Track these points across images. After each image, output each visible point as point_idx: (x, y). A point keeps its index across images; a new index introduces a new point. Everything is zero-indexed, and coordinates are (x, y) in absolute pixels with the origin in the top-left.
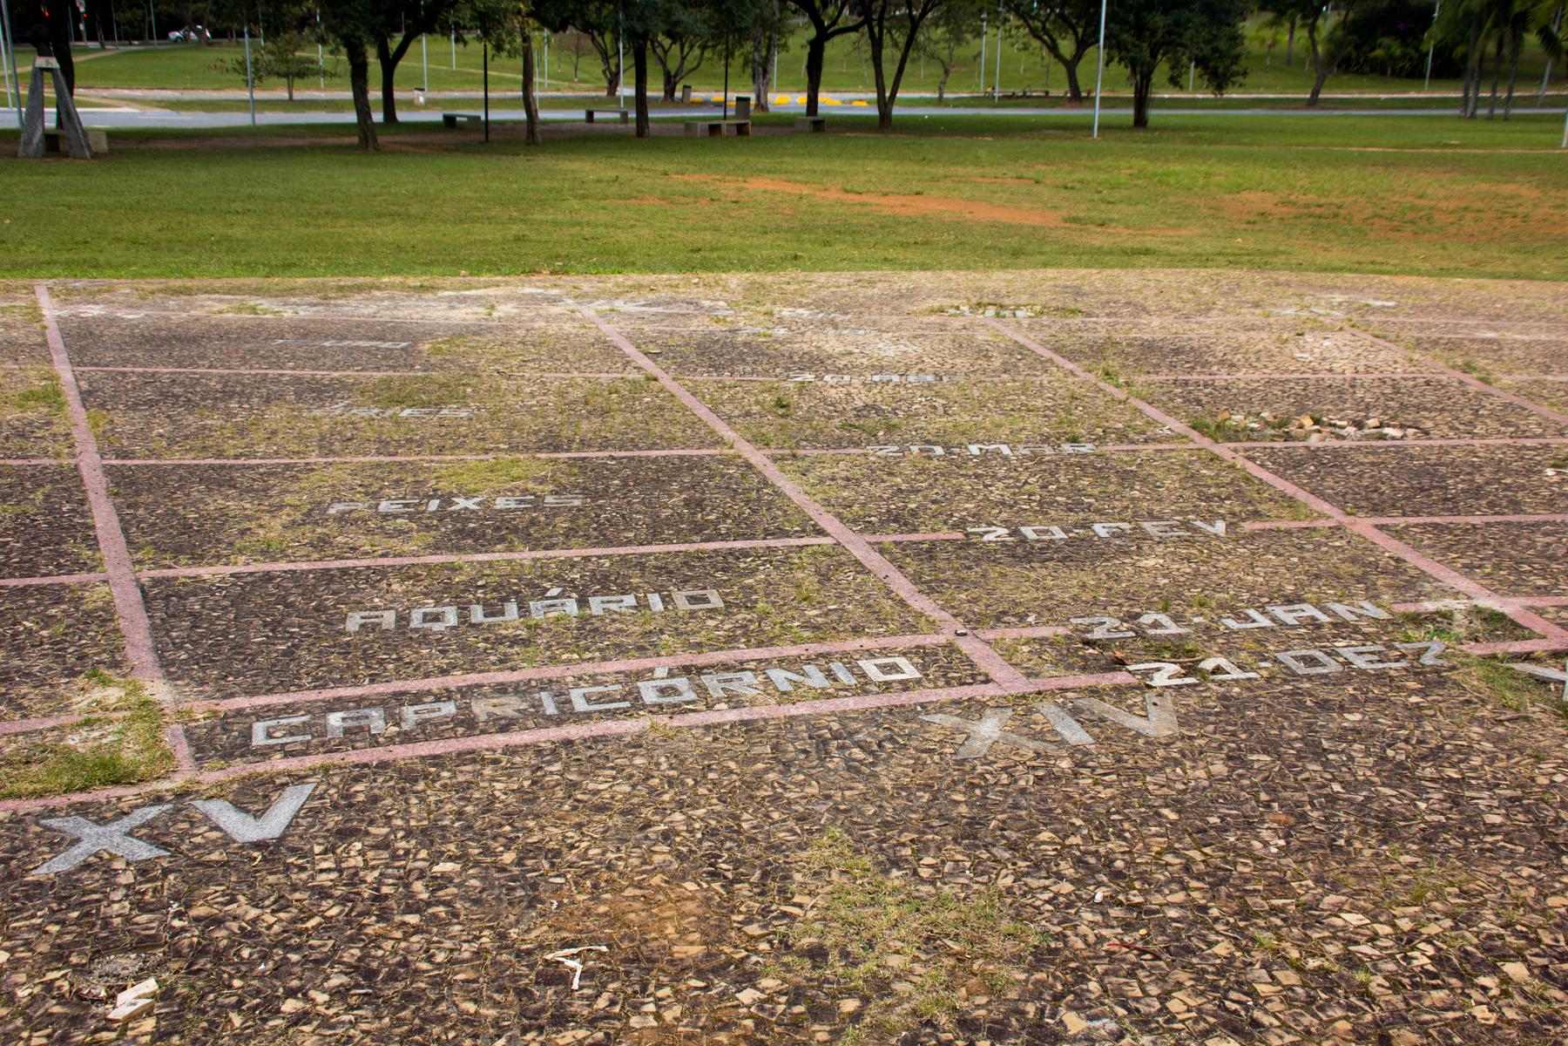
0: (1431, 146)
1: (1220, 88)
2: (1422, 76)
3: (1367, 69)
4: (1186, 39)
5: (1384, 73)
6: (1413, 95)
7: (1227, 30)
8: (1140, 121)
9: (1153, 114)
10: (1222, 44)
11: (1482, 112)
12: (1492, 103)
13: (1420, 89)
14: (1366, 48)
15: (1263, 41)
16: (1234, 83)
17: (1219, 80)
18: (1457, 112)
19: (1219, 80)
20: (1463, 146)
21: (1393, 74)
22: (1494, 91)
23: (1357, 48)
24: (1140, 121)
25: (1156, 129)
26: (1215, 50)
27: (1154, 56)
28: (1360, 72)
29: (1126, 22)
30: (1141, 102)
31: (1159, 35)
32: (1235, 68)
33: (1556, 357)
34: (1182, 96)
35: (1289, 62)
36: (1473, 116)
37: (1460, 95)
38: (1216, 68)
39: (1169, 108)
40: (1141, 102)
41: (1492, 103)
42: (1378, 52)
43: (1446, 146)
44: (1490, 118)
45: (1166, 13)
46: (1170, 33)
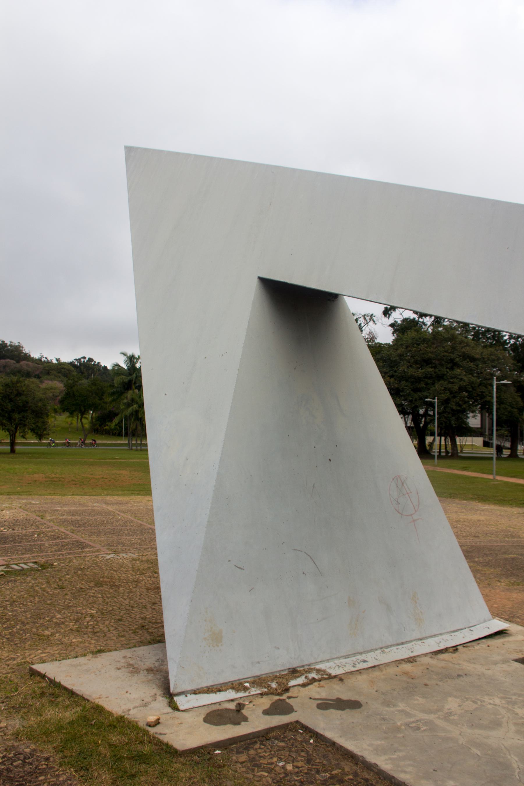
0: (110, 459)
1: (40, 439)
2: (122, 436)
3: (104, 433)
4: (26, 423)
5: (110, 434)
6: (119, 442)
7: (41, 420)
8: (13, 451)
9: (17, 448)
10: (39, 425)
11: (134, 448)
12: (136, 445)
13: (121, 440)
14: (103, 426)
15: (67, 423)
16: (45, 438)
17: (40, 437)
18: (127, 448)
19: (40, 437)
20: (120, 459)
21: (113, 435)
22: (137, 441)
23: (100, 426)
24: (13, 451)
25: (18, 453)
26: (37, 426)
27: (16, 428)
28: (102, 434)
29: (5, 416)
30: (13, 444)
31: (17, 421)
32: (45, 432)
33: (522, 555)
34: (28, 442)
35: (77, 430)
36: (132, 449)
37: (127, 442)
38: (38, 432)
39: (32, 446)
40: (13, 444)
41: (136, 445)
42: (107, 427)
43: (440, 444)
44: (137, 450)
45: (19, 413)
46: (21, 420)
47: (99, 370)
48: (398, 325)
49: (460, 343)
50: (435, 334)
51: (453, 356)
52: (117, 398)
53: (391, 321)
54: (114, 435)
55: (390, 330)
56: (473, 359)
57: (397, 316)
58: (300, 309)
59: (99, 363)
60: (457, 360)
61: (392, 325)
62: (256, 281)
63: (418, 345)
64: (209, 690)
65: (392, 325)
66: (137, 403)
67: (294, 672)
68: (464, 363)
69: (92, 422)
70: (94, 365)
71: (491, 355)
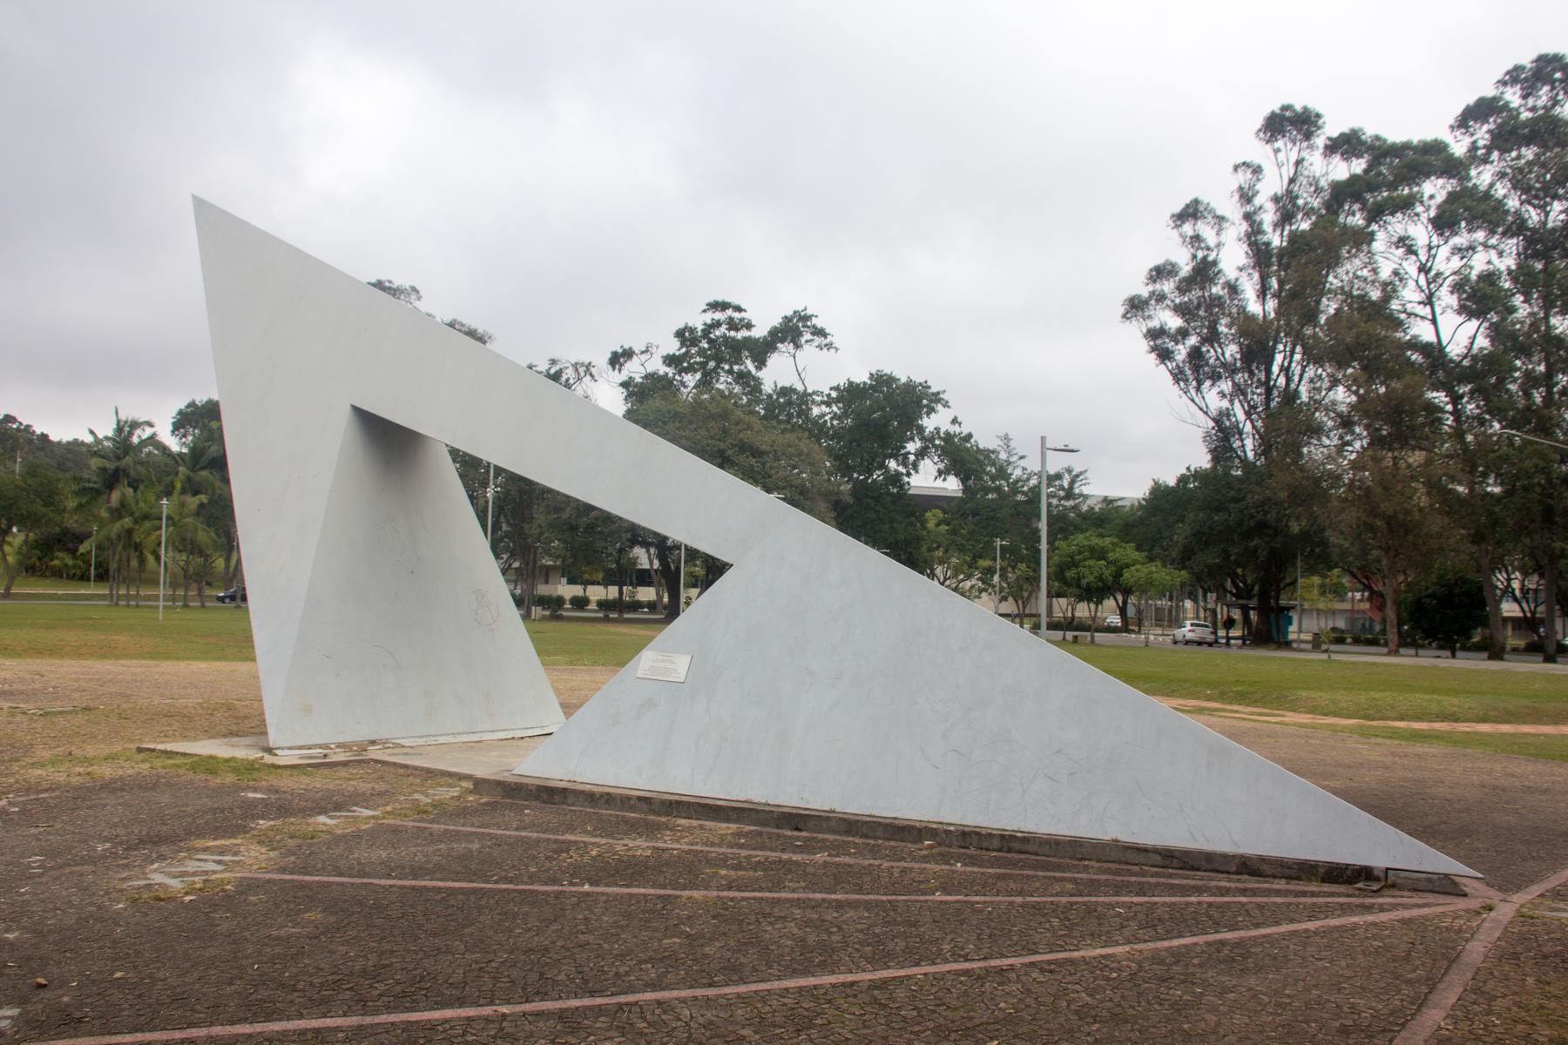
2: (89, 580)
12: (128, 597)
28: (43, 576)
41: (128, 597)
42: (56, 562)
47: (31, 442)
48: (636, 385)
49: (737, 424)
50: (697, 404)
51: (722, 446)
52: (88, 503)
53: (623, 377)
54: (72, 577)
55: (621, 393)
56: (757, 453)
57: (635, 369)
58: (388, 442)
59: (28, 426)
60: (730, 452)
61: (625, 385)
62: (348, 410)
63: (665, 423)
64: (301, 748)
65: (625, 385)
66: (132, 514)
67: (373, 742)
68: (741, 458)
69: (19, 552)
70: (18, 429)
71: (789, 446)
